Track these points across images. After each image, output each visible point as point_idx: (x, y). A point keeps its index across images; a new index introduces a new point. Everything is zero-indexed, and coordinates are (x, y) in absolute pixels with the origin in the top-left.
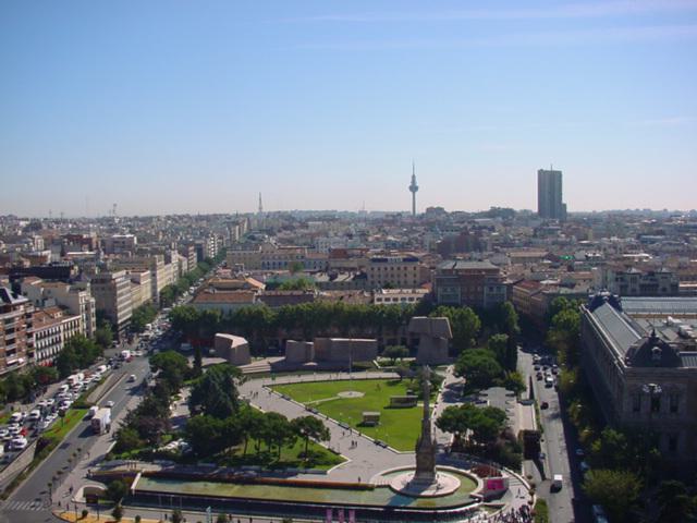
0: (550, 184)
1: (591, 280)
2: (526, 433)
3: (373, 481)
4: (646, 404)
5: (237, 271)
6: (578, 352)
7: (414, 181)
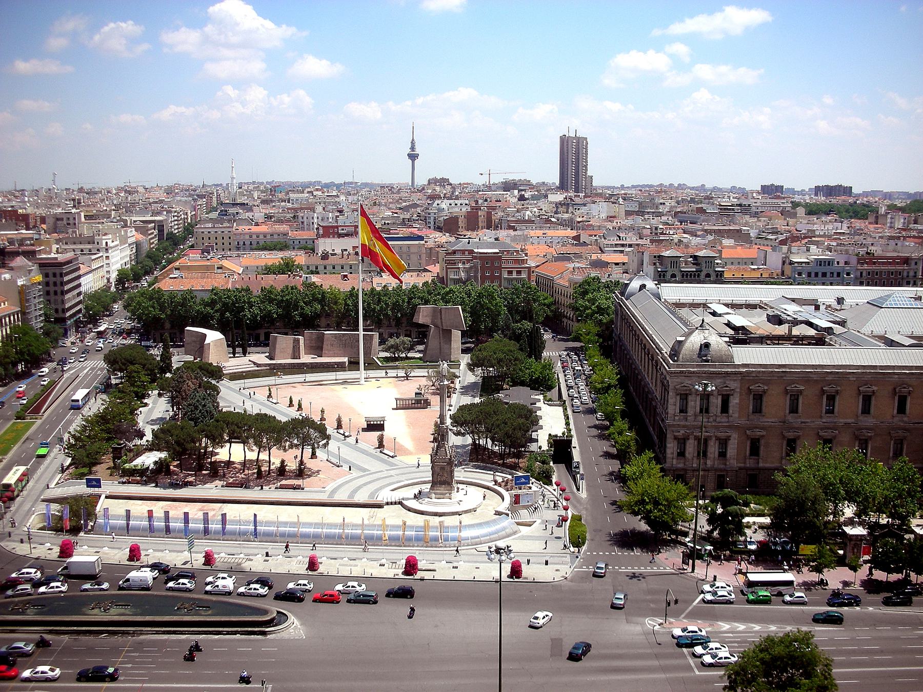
0: (573, 154)
1: (624, 264)
2: (796, 213)
3: (385, 496)
4: (694, 404)
5: (209, 253)
6: (614, 339)
7: (413, 148)
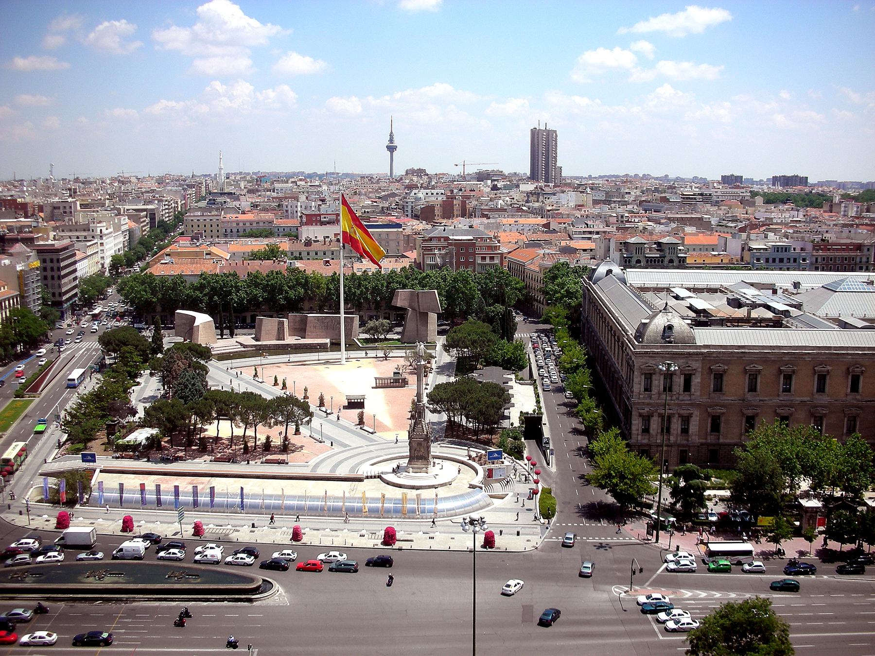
0: (543, 146)
1: (591, 250)
3: (365, 470)
4: (658, 383)
5: (198, 240)
6: (582, 321)
7: (391, 141)
